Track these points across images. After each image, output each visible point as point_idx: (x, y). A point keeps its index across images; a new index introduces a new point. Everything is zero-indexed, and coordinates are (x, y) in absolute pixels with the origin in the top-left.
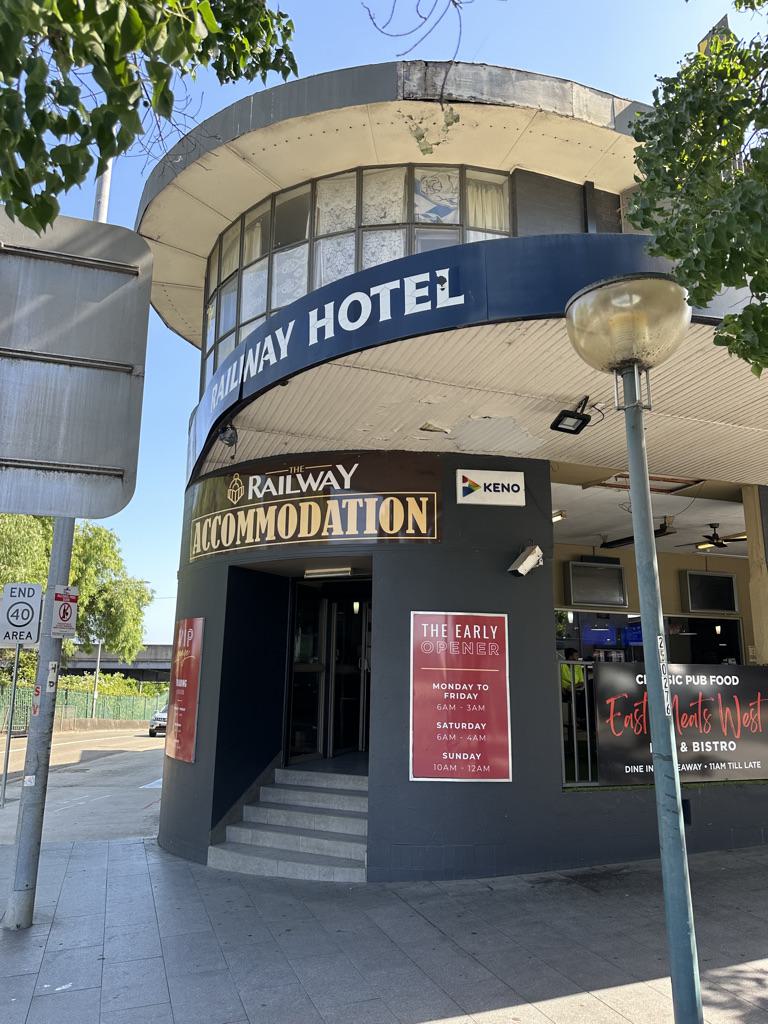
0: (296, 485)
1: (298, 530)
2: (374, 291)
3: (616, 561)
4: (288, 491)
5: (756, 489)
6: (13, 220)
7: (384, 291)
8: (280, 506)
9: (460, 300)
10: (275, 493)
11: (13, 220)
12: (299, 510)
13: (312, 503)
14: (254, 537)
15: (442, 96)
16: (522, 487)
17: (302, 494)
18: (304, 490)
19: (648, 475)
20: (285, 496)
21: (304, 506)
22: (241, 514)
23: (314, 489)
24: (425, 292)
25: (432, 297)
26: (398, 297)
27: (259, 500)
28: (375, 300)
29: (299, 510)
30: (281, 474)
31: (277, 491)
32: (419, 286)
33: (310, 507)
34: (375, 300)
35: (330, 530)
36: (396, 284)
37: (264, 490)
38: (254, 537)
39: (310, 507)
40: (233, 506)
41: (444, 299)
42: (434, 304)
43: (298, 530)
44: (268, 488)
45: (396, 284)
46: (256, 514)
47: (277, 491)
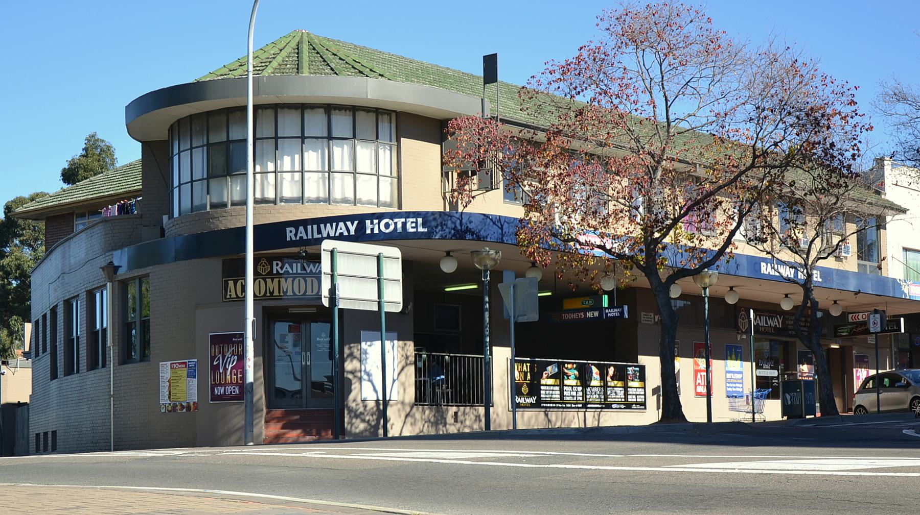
0: (304, 268)
1: (306, 291)
2: (396, 220)
3: (38, 435)
4: (299, 271)
5: (255, 253)
6: (679, 371)
7: (400, 221)
8: (294, 279)
9: (426, 230)
10: (291, 272)
11: (679, 371)
12: (306, 281)
13: (313, 279)
14: (279, 292)
15: (601, 387)
16: (401, 280)
17: (307, 273)
18: (308, 271)
19: (888, 370)
20: (297, 273)
21: (309, 280)
22: (269, 281)
23: (314, 272)
24: (414, 225)
25: (416, 227)
26: (404, 224)
27: (281, 274)
28: (396, 224)
29: (306, 281)
30: (294, 263)
31: (292, 271)
32: (412, 222)
33: (312, 280)
34: (396, 224)
35: (230, 295)
36: (403, 220)
37: (284, 269)
38: (279, 292)
39: (312, 280)
40: (263, 275)
41: (421, 229)
42: (417, 230)
43: (306, 291)
44: (286, 268)
45: (403, 220)
46: (279, 281)
47: (292, 271)
